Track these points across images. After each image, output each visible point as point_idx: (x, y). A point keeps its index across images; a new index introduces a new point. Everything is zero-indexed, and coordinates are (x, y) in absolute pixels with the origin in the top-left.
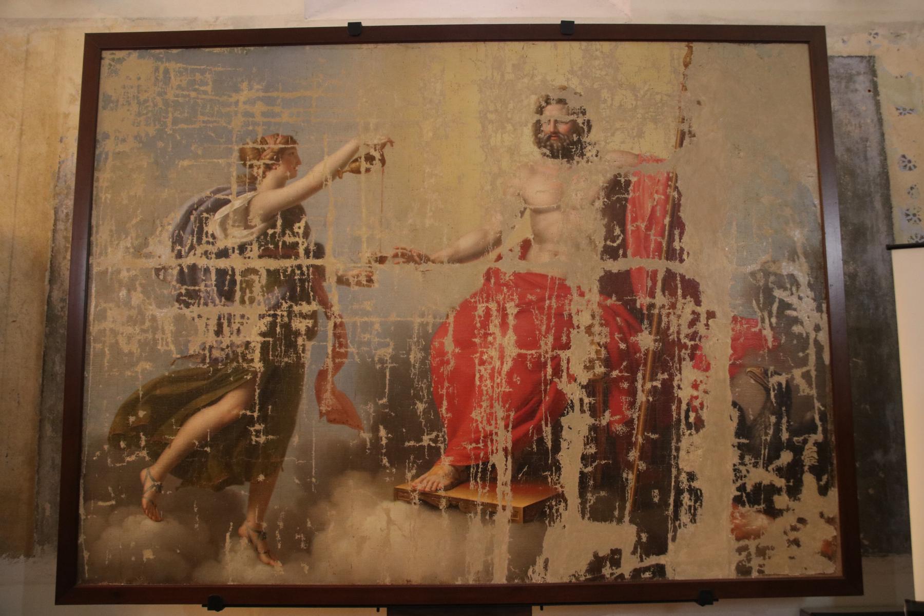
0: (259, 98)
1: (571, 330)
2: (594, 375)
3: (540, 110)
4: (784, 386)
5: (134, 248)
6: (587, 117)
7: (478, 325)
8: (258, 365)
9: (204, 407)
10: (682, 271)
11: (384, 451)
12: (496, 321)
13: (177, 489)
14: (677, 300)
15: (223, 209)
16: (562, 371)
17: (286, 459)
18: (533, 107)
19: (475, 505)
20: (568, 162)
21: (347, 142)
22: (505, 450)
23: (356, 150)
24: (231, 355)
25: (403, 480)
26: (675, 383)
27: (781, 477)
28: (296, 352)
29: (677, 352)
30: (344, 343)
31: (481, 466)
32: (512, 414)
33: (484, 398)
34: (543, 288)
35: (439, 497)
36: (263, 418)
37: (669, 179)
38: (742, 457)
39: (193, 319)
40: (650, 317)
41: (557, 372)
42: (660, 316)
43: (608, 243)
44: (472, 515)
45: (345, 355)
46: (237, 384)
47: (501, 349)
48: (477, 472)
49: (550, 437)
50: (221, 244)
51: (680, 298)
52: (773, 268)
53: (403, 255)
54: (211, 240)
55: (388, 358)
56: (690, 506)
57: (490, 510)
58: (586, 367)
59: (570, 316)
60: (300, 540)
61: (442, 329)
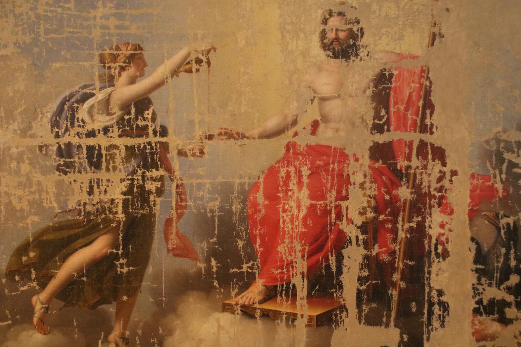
0: (111, 14)
1: (349, 186)
2: (366, 219)
3: (325, 22)
4: (512, 225)
5: (20, 130)
6: (360, 26)
7: (281, 184)
8: (121, 216)
9: (81, 248)
10: (432, 141)
11: (215, 276)
12: (294, 180)
13: (61, 309)
14: (428, 163)
15: (90, 100)
16: (343, 216)
17: (143, 284)
18: (320, 19)
19: (281, 314)
20: (346, 61)
21: (181, 49)
22: (302, 274)
23: (189, 55)
24: (100, 209)
25: (229, 297)
26: (427, 224)
27: (510, 294)
28: (149, 206)
29: (428, 201)
30: (184, 198)
31: (285, 286)
32: (307, 248)
33: (286, 236)
34: (328, 156)
35: (255, 309)
36: (126, 255)
37: (423, 71)
38: (479, 279)
39: (70, 183)
40: (408, 175)
41: (339, 217)
42: (415, 174)
43: (376, 121)
44: (279, 321)
45: (185, 207)
46: (106, 230)
47: (298, 201)
48: (282, 290)
49: (334, 264)
50: (89, 127)
51: (430, 161)
52: (504, 137)
53: (226, 134)
54: (81, 124)
55: (216, 209)
56: (440, 315)
57: (292, 318)
58: (360, 213)
59: (348, 175)
60: (154, 343)
61: (255, 187)
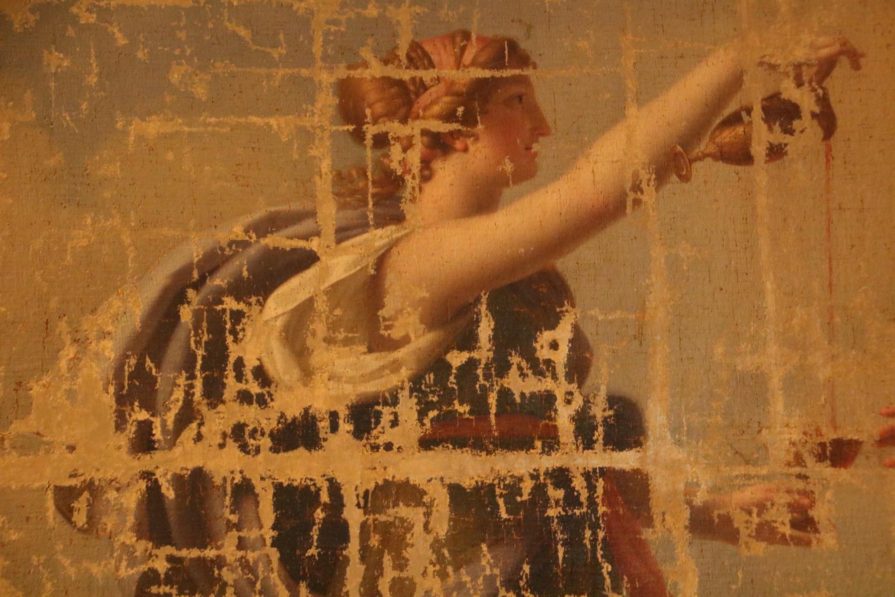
21: (701, 57)
50: (290, 403)
54: (255, 388)
